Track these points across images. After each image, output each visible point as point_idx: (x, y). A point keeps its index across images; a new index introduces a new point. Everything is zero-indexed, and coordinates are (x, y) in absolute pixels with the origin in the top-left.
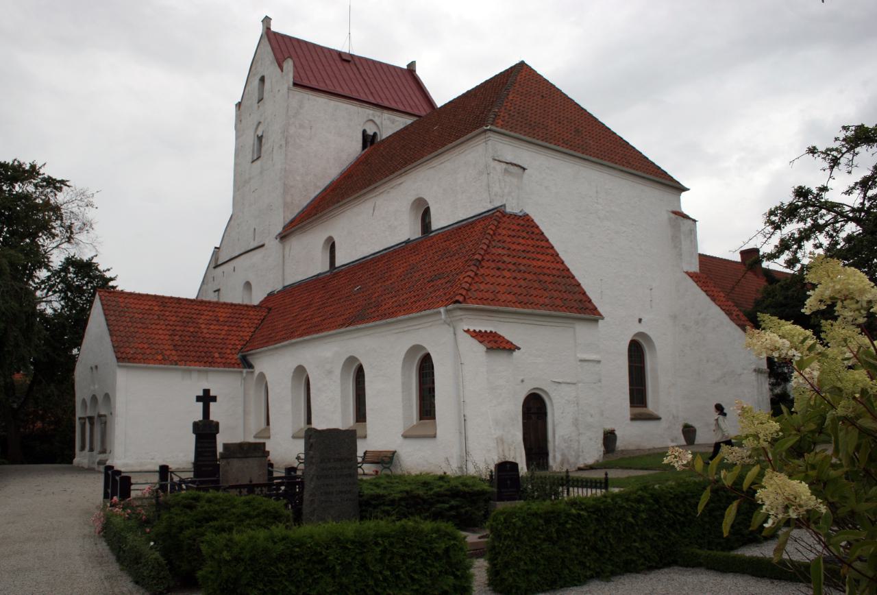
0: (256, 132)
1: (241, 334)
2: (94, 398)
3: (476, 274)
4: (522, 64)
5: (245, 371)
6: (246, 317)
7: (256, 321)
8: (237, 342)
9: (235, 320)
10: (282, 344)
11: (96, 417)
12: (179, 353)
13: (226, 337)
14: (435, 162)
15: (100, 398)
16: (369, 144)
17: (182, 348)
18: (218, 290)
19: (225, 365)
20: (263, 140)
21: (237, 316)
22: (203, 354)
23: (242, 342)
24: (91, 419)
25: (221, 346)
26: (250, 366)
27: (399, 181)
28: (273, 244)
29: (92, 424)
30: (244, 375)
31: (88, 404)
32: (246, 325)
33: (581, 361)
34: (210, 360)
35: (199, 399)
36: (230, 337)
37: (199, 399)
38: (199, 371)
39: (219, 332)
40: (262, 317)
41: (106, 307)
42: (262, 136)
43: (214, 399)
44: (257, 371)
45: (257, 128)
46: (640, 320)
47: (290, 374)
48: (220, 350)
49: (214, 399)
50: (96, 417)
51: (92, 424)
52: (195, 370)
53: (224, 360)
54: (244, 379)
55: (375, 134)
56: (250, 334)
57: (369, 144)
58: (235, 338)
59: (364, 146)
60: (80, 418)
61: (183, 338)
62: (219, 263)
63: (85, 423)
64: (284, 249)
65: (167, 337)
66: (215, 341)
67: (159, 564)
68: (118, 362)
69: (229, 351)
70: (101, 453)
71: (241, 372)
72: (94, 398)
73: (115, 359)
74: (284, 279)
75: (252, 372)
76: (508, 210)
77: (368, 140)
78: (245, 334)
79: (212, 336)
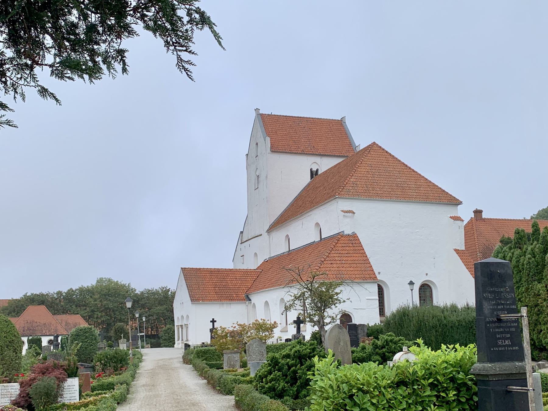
0: (256, 173)
1: (247, 284)
2: (182, 317)
3: (320, 267)
4: (374, 143)
5: (247, 302)
6: (250, 275)
7: (255, 277)
8: (245, 289)
9: (244, 278)
10: (262, 290)
11: (184, 325)
12: (218, 296)
13: (239, 286)
14: (322, 208)
15: (185, 317)
16: (314, 175)
17: (219, 294)
18: (243, 256)
19: (238, 300)
20: (259, 176)
21: (245, 275)
22: (229, 296)
23: (247, 289)
24: (182, 326)
25: (237, 291)
26: (250, 300)
27: (310, 213)
28: (265, 235)
29: (182, 328)
30: (247, 304)
31: (180, 319)
32: (249, 280)
33: (367, 300)
34: (232, 298)
35: (211, 322)
36: (241, 286)
37: (211, 322)
38: (227, 303)
39: (236, 284)
40: (258, 275)
41: (186, 279)
42: (259, 176)
43: (216, 321)
44: (253, 301)
45: (256, 173)
46: (427, 274)
47: (264, 304)
48: (236, 293)
49: (216, 321)
50: (184, 325)
51: (182, 328)
52: (225, 303)
53: (238, 298)
54: (247, 306)
55: (317, 170)
56: (251, 284)
57: (314, 175)
58: (244, 287)
59: (312, 177)
60: (177, 326)
61: (220, 288)
62: (243, 242)
63: (179, 328)
64: (269, 238)
65: (213, 289)
66: (234, 289)
67: (128, 285)
68: (192, 301)
69: (240, 293)
70: (186, 341)
71: (246, 303)
72: (182, 317)
73: (190, 300)
74: (270, 253)
75: (251, 303)
76: (346, 233)
77: (314, 174)
78: (249, 284)
79: (233, 286)
